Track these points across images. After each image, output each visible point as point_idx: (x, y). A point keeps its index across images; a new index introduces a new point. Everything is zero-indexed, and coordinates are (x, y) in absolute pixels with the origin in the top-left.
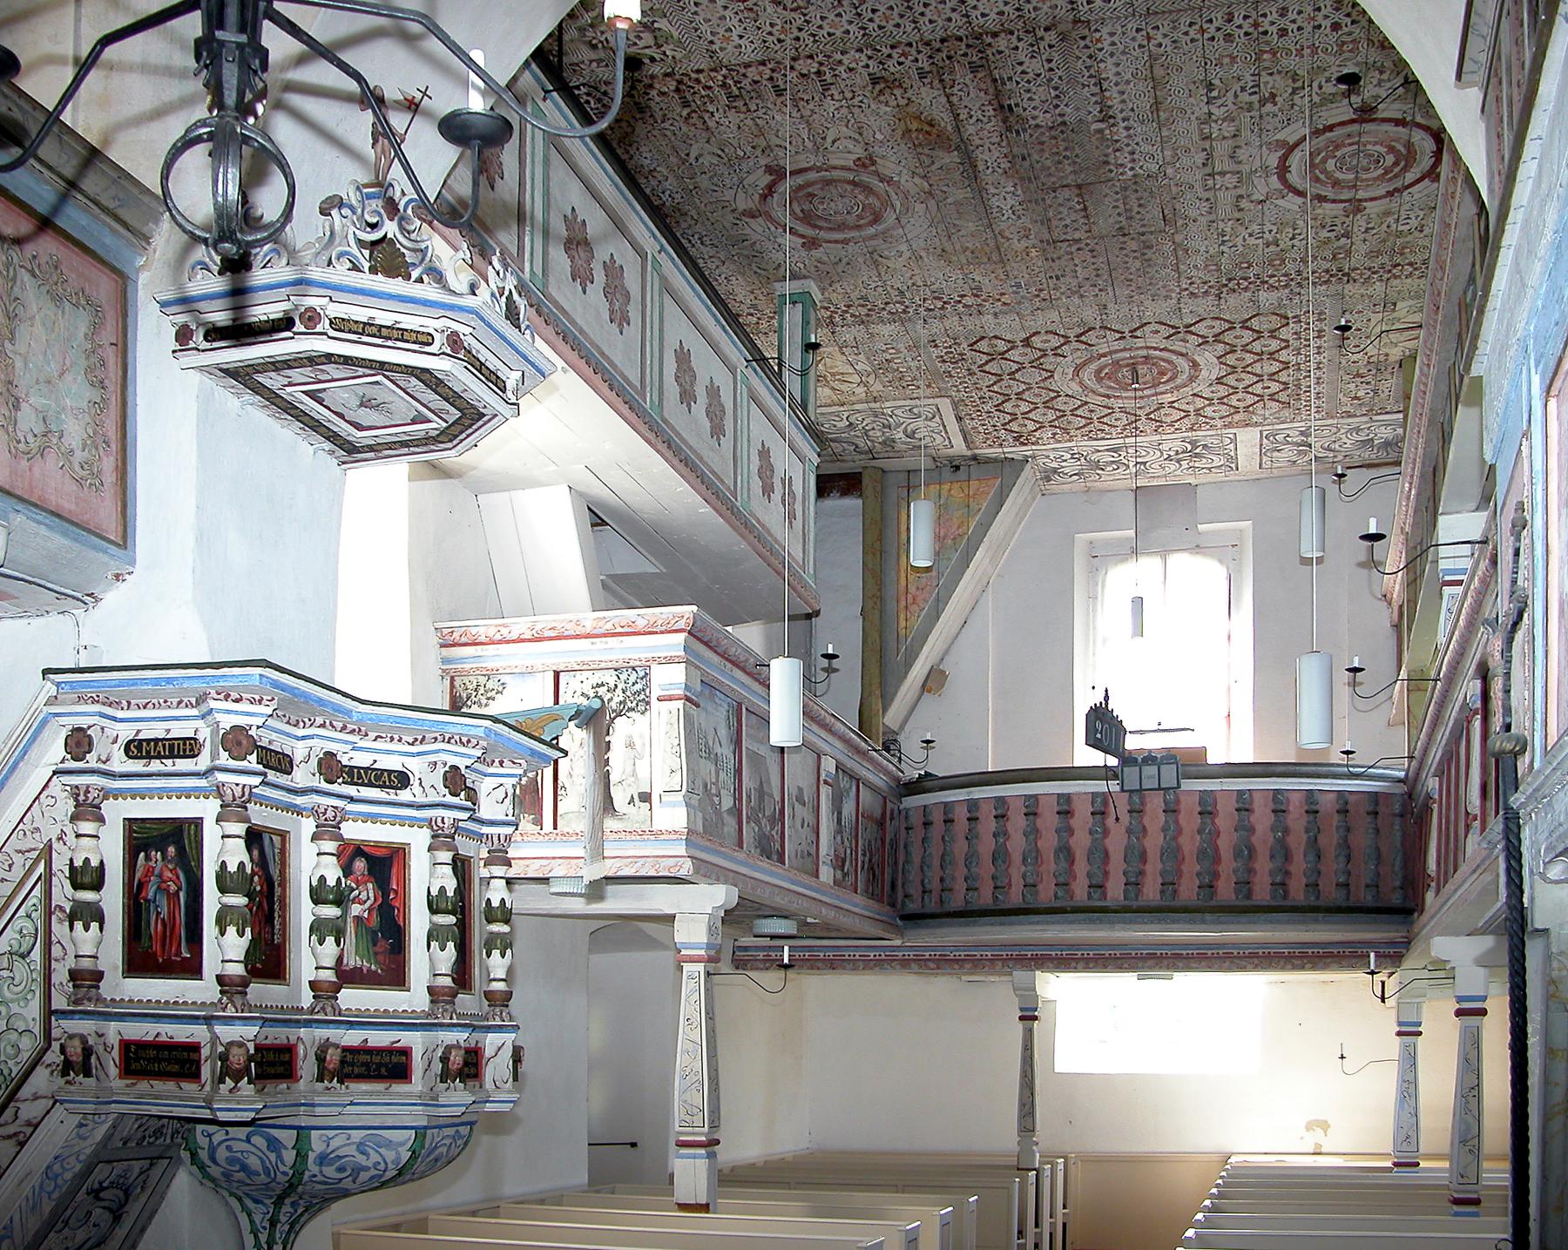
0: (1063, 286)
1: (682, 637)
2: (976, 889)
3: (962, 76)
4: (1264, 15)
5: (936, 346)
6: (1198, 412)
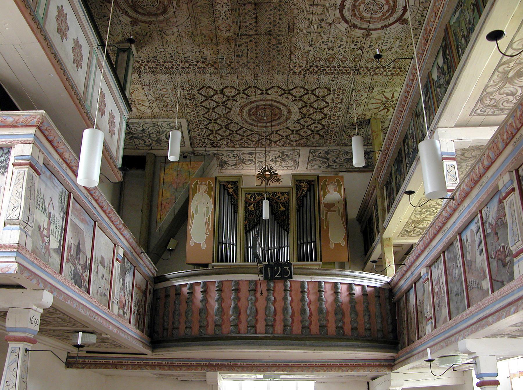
0: (241, 61)
1: (32, 131)
2: (191, 328)
5: (183, 89)
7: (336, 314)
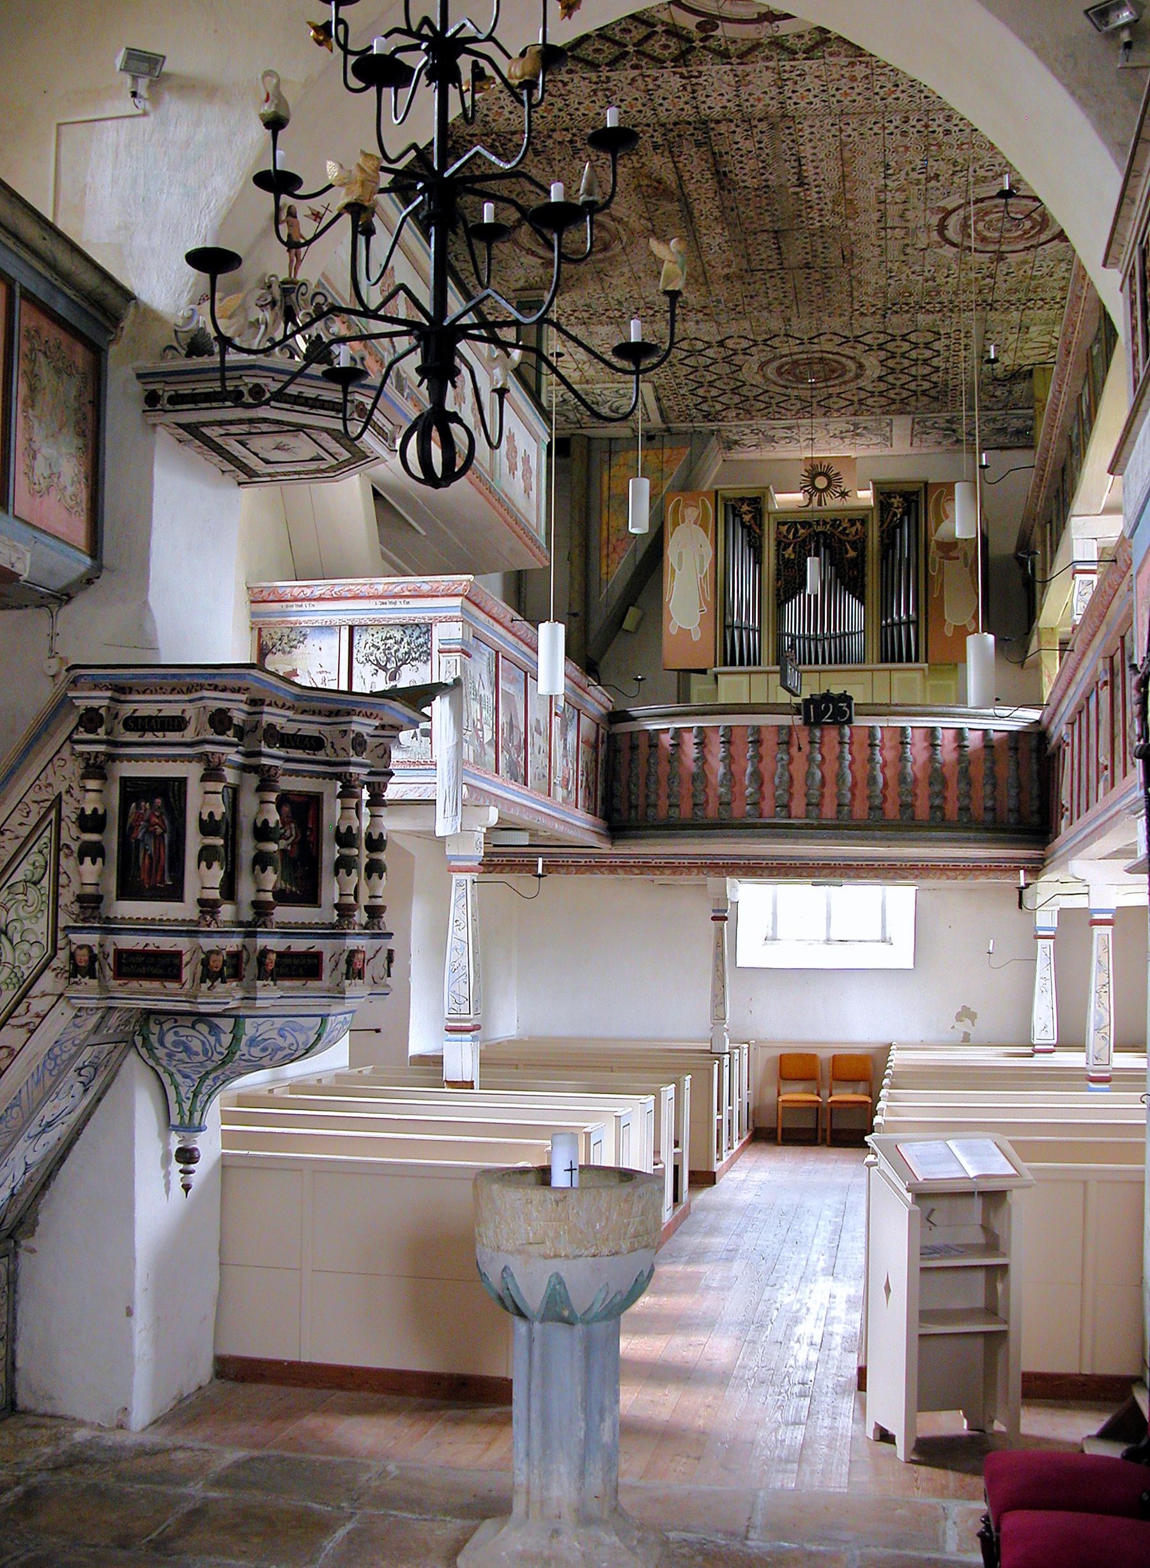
1: (457, 601)
2: (678, 806)
3: (688, 148)
4: (934, 120)
6: (861, 402)
7: (930, 784)
